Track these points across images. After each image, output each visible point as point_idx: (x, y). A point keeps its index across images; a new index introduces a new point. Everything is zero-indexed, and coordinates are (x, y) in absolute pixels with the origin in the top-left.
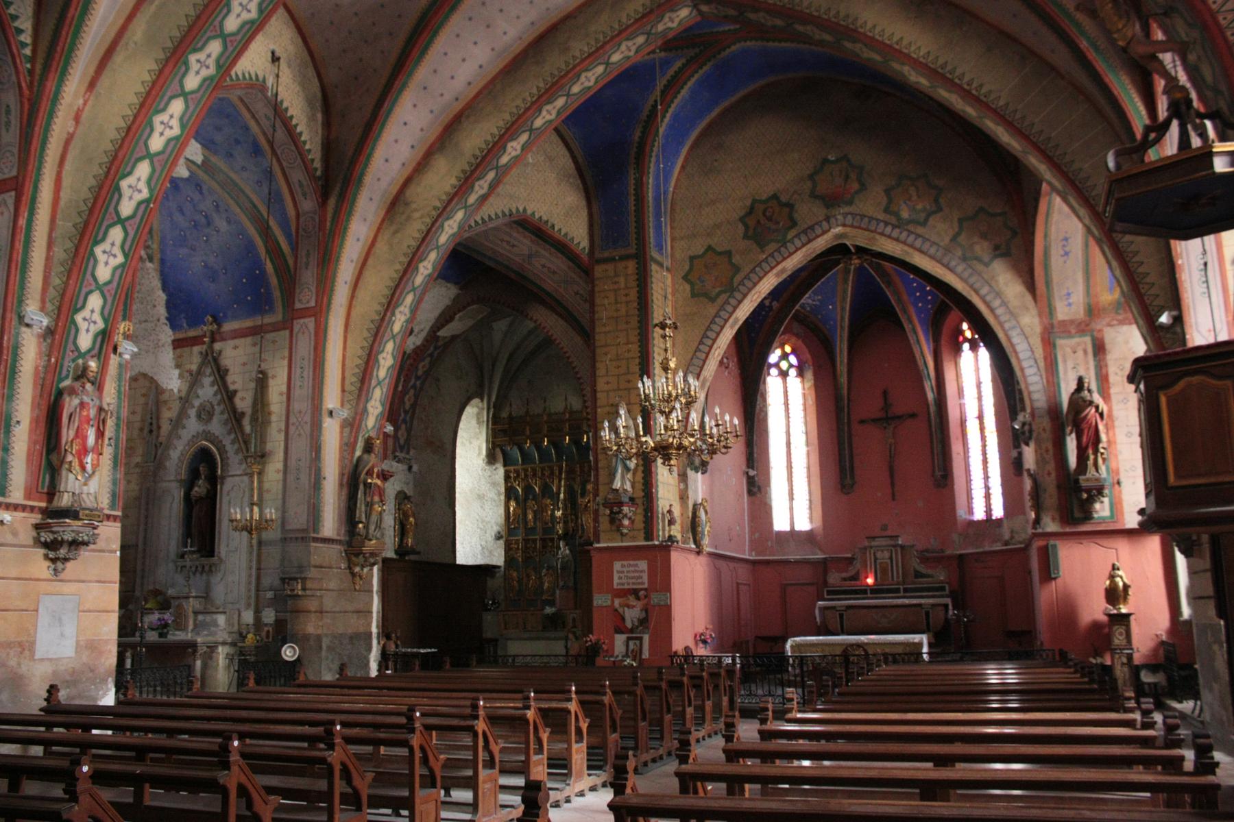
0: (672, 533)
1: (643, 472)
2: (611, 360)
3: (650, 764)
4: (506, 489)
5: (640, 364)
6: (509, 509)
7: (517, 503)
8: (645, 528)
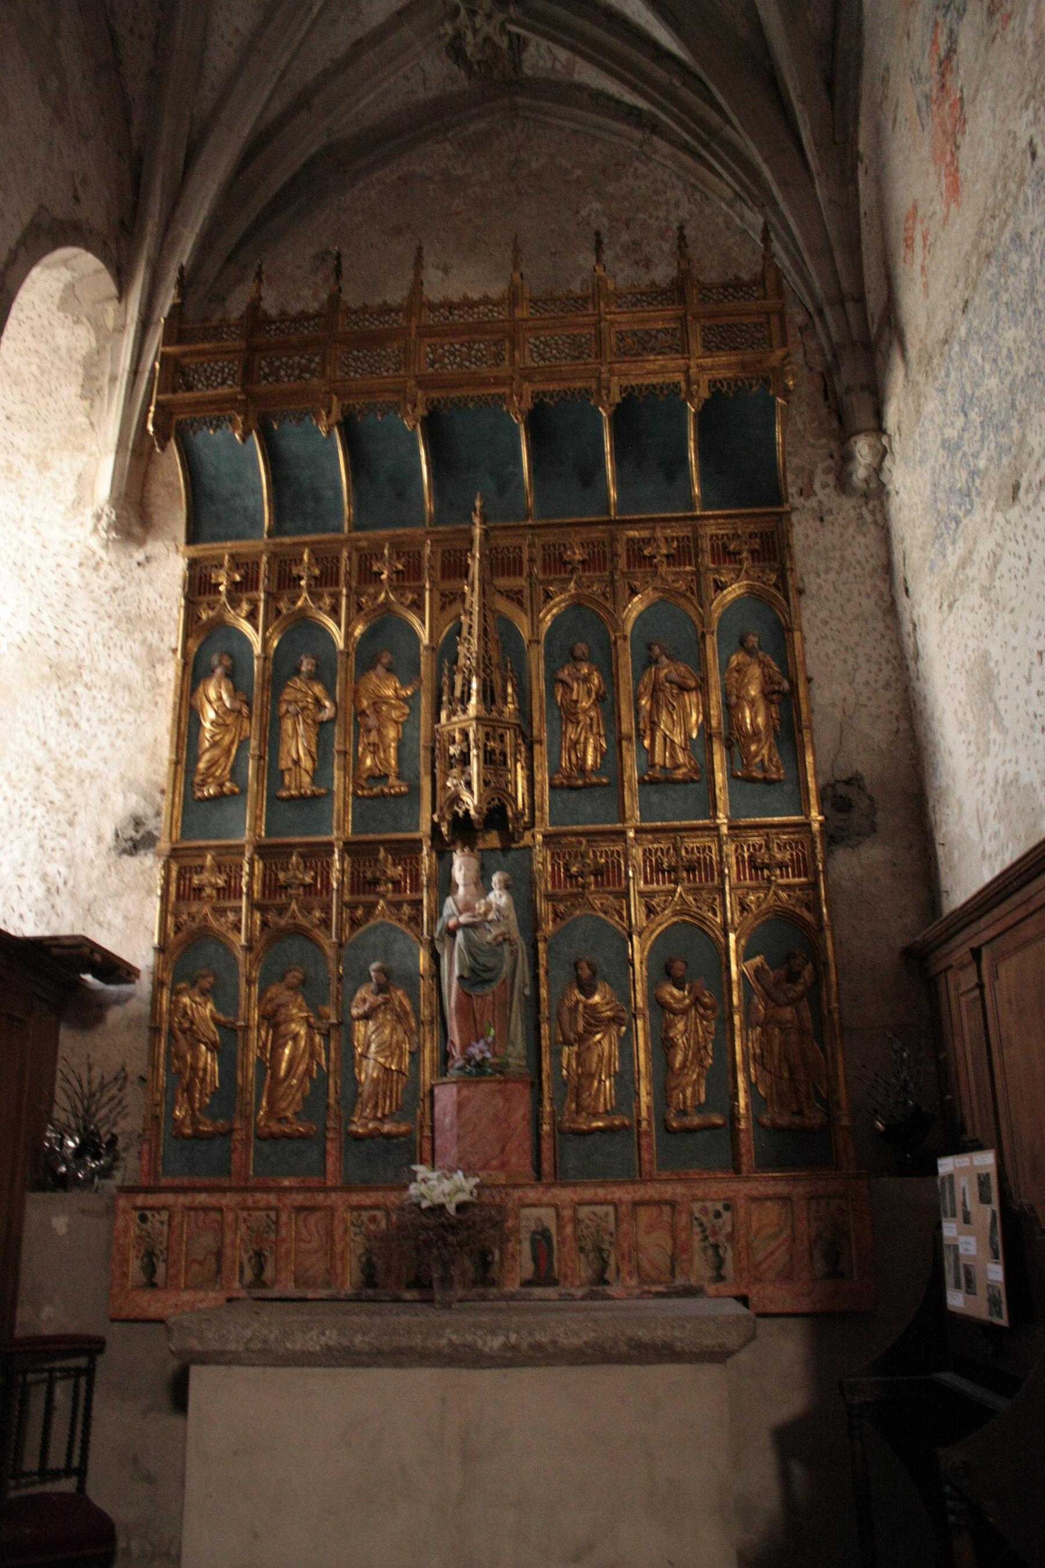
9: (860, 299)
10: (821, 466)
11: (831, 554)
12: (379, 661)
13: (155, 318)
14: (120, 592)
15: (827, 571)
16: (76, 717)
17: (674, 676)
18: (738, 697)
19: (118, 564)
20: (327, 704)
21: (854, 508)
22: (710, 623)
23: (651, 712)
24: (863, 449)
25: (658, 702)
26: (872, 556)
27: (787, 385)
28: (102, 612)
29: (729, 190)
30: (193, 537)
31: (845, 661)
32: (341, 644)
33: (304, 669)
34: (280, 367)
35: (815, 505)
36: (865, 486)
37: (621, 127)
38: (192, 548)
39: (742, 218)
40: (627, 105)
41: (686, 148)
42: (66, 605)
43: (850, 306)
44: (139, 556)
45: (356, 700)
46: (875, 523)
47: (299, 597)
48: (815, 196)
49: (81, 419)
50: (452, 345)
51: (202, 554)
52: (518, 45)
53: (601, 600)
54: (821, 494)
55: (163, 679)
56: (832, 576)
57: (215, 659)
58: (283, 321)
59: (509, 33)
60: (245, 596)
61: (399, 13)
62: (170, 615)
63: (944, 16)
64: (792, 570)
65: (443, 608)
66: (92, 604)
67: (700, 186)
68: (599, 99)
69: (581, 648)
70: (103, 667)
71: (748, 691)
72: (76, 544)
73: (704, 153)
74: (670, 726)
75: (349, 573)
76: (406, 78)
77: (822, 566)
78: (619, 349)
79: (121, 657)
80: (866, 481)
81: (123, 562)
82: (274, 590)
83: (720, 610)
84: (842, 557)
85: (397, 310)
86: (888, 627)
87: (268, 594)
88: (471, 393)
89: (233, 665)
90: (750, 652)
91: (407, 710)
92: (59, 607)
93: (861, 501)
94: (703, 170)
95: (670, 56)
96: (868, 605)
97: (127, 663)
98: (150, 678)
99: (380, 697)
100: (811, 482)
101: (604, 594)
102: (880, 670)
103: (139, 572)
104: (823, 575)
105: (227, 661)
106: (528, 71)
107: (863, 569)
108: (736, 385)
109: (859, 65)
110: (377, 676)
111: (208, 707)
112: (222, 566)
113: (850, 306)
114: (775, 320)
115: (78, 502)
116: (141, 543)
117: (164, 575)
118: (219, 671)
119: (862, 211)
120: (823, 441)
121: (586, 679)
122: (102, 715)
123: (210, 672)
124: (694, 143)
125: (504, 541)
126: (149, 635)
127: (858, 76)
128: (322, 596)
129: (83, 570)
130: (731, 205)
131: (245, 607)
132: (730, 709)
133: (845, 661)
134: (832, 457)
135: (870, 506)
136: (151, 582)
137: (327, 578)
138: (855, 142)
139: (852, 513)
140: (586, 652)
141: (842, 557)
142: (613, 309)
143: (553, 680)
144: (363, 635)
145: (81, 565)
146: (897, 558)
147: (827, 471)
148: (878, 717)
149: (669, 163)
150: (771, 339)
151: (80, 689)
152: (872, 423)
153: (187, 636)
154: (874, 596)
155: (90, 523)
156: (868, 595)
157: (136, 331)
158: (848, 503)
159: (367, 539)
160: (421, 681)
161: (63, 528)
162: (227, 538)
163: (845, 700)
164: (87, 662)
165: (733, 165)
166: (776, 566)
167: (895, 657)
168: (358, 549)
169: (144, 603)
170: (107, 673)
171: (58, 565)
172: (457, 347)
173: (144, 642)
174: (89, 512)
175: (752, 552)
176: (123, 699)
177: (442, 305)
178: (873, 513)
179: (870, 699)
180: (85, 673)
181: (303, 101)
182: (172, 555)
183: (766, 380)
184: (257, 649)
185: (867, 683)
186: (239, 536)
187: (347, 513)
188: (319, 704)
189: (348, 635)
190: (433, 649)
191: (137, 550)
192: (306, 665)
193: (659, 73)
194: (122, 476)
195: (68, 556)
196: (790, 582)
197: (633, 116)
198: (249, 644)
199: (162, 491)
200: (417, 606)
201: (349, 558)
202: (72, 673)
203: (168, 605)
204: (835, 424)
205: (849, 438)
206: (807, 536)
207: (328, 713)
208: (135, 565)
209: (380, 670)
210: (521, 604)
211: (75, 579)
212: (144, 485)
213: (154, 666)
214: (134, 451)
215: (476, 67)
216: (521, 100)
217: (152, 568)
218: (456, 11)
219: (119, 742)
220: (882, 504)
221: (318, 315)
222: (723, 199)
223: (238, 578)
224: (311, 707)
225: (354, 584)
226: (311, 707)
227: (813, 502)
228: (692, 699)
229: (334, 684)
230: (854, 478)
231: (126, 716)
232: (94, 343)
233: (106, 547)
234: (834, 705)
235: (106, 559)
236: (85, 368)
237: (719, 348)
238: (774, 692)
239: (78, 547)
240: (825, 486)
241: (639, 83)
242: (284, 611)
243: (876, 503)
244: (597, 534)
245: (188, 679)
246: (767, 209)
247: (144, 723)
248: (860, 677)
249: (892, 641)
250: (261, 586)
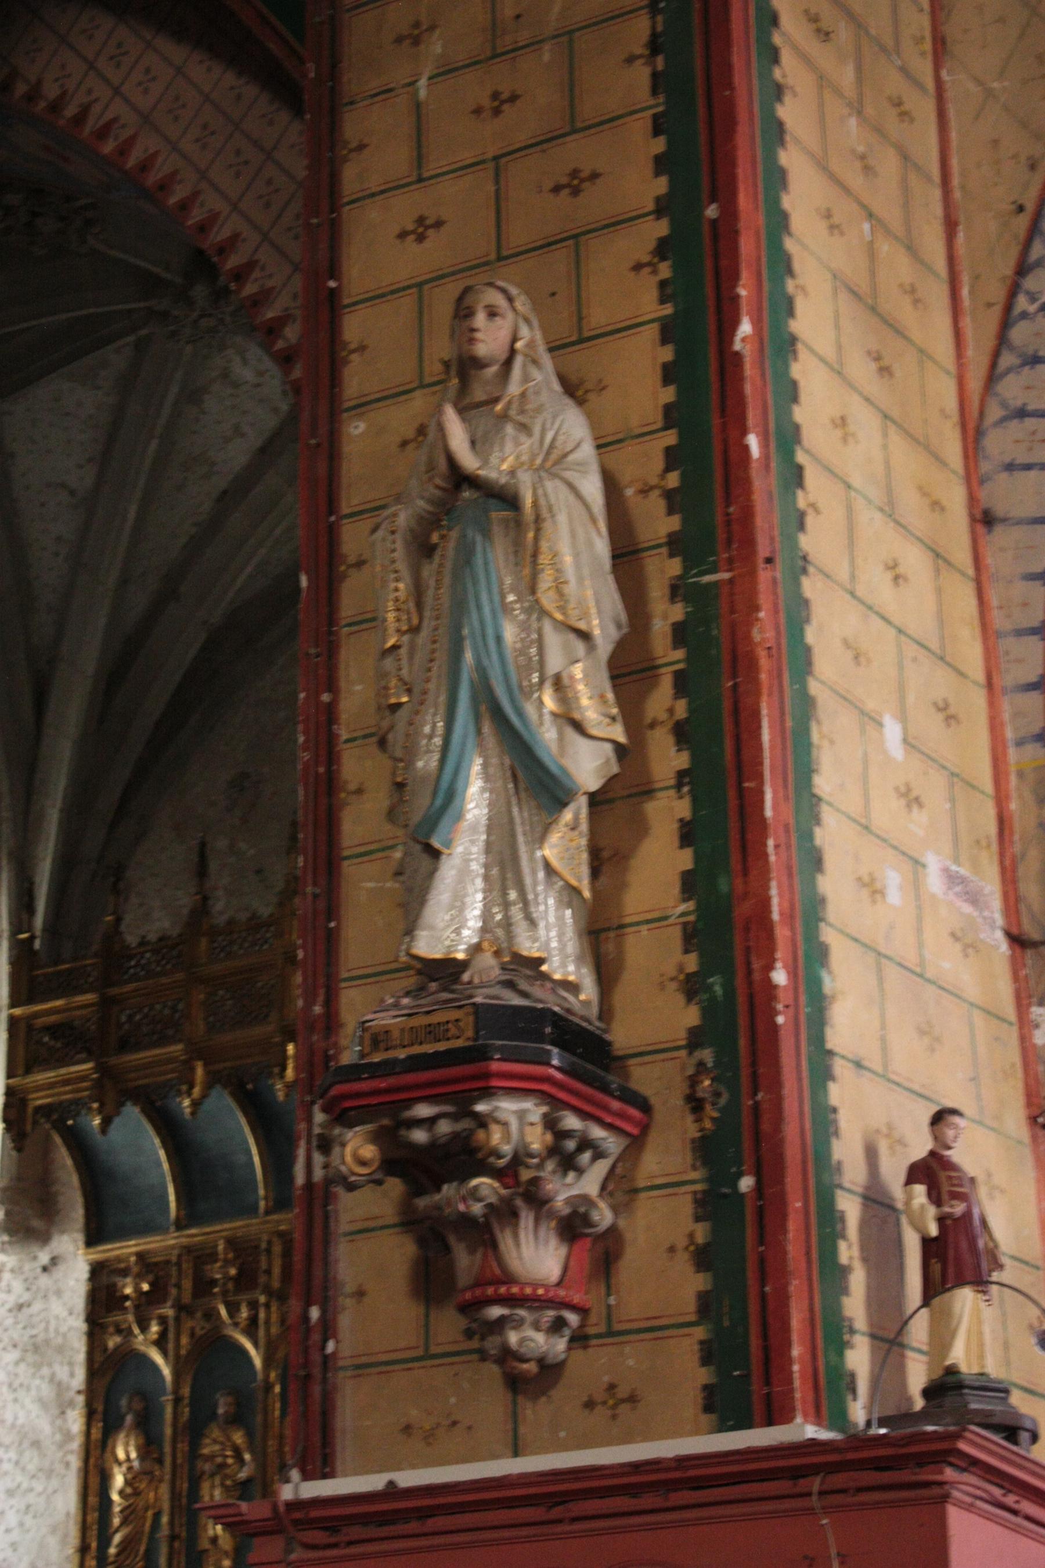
0: (959, 1355)
1: (687, 835)
2: (446, 71)
3: (814, 26)
4: (93, 1371)
5: (655, 46)
6: (105, 1479)
7: (150, 1447)
8: (706, 1305)
33: (221, 1411)
38: (91, 1250)
57: (124, 1402)
61: (262, 450)
63: (16, 1418)
81: (27, 1267)
97: (35, 1409)
98: (60, 1429)
103: (44, 1281)
118: (129, 1419)
126: (57, 1368)
136: (59, 1293)
137: (246, 1280)
170: (13, 1426)
173: (52, 1378)
176: (32, 1461)
208: (39, 1270)
217: (58, 1272)
219: (29, 1521)
223: (145, 1287)
247: (55, 1492)
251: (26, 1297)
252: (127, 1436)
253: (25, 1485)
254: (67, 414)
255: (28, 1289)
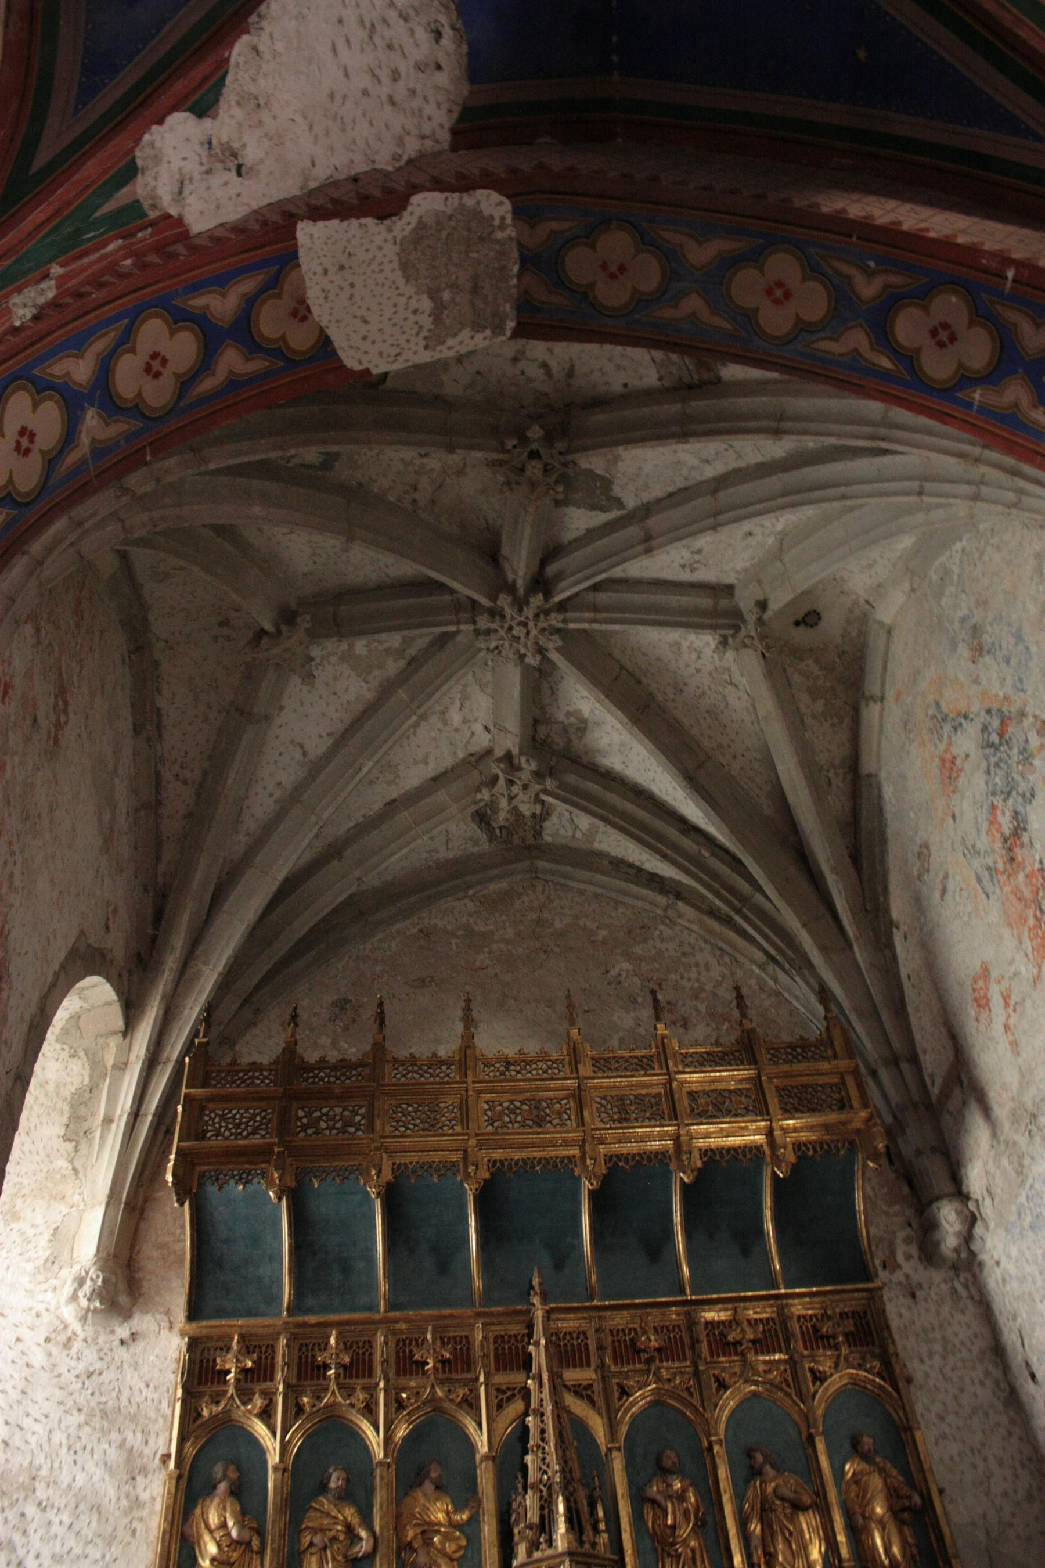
9: (914, 1059)
10: (901, 1235)
11: (931, 1336)
12: (427, 1476)
13: (164, 1057)
14: (95, 1376)
15: (931, 1354)
16: (21, 1552)
17: (786, 1492)
18: (864, 1517)
19: (95, 1340)
20: (363, 1534)
21: (945, 1281)
22: (815, 1421)
23: (763, 1539)
24: (948, 1216)
25: (770, 1526)
26: (976, 1336)
27: (876, 1148)
28: (70, 1403)
29: (761, 954)
30: (194, 1313)
31: (974, 1467)
32: (379, 1453)
33: (332, 1485)
34: (320, 1118)
35: (903, 1279)
36: (955, 1255)
37: (644, 892)
38: (194, 1325)
39: (775, 980)
40: (648, 872)
41: (712, 913)
42: (24, 1392)
43: (905, 1066)
44: (123, 1331)
45: (399, 1529)
46: (971, 1298)
47: (326, 1389)
48: (855, 960)
49: (62, 1164)
50: (512, 1102)
51: (205, 1332)
52: (547, 812)
53: (685, 1395)
54: (907, 1267)
55: (145, 1496)
56: (937, 1361)
57: (218, 1470)
58: (321, 1069)
59: (543, 802)
60: (258, 1387)
61: (434, 779)
62: (158, 1410)
63: (1004, 800)
64: (897, 1355)
65: (500, 1407)
66: (58, 1392)
67: (727, 948)
68: (620, 866)
69: (670, 1458)
70: (65, 1479)
71: (873, 1510)
72: (44, 1314)
73: (737, 918)
74: (789, 1558)
75: (385, 1361)
76: (432, 839)
77: (924, 1350)
78: (693, 1110)
79: (90, 1466)
80: (956, 1250)
82: (294, 1381)
83: (823, 1406)
84: (943, 1338)
85: (448, 1063)
86: (1012, 1422)
87: (287, 1385)
88: (538, 1155)
89: (239, 1478)
90: (866, 1457)
91: (464, 1543)
92: (14, 1395)
93: (951, 1273)
94: (731, 935)
95: (697, 830)
96: (985, 1394)
97: (99, 1473)
98: (128, 1496)
99: (430, 1523)
100: (893, 1253)
101: (688, 1389)
102: (1017, 1476)
103: (121, 1353)
104: (926, 1360)
105: (233, 1474)
106: (548, 839)
107: (970, 1351)
108: (822, 1148)
109: (884, 841)
110: (425, 1495)
111: (207, 1538)
112: (229, 1349)
113: (905, 1066)
114: (850, 1081)
115: (52, 1261)
116: (126, 1315)
117: (152, 1358)
118: (222, 1487)
119: (904, 974)
120: (897, 1208)
121: (681, 1497)
122: (58, 1549)
123: (209, 1489)
124: (725, 908)
125: (568, 1324)
126: (130, 1436)
127: (884, 852)
128: (354, 1390)
129: (50, 1346)
130: (762, 967)
131: (258, 1402)
132: (857, 1533)
133: (974, 1467)
134: (910, 1225)
135: (962, 1279)
136: (135, 1366)
138: (887, 910)
139: (944, 1286)
140: (676, 1460)
141: (943, 1338)
142: (680, 1068)
143: (640, 1499)
144: (405, 1439)
145: (47, 1340)
146: (1010, 1337)
147: (908, 1241)
148: (1029, 1539)
149: (695, 927)
150: (850, 1101)
151: (31, 1510)
152: (950, 1188)
153: (182, 1439)
154: (989, 1383)
155: (68, 1289)
156: (982, 1383)
157: (142, 1070)
158: (938, 1276)
159: (407, 1320)
160: (479, 1503)
161: (30, 1292)
162: (235, 1314)
163: (985, 1516)
164: (44, 1472)
165: (767, 930)
166: (877, 1351)
167: (1030, 1460)
168: (394, 1332)
169: (126, 1393)
170: (69, 1487)
171: (18, 1340)
172: (518, 1104)
174: (67, 1276)
175: (846, 1335)
176: (89, 1526)
177: (498, 1060)
178: (966, 1286)
179: (1013, 1515)
180: (40, 1486)
181: (334, 851)
182: (165, 1333)
183: (852, 1143)
184: (273, 1458)
185: (1005, 1494)
186: (250, 1313)
187: (383, 1289)
188: (352, 1537)
189: (388, 1439)
190: (494, 1459)
191: (121, 1325)
192: (335, 1481)
193: (688, 843)
194: (112, 1233)
195: (32, 1328)
196: (897, 1371)
197: (655, 881)
198: (261, 1451)
199: (155, 1254)
200: (470, 1404)
201: (386, 1343)
202: (22, 1486)
203: (156, 1396)
204: (906, 1190)
205: (930, 1203)
206: (901, 1316)
207: (364, 1546)
208: (117, 1342)
209: (428, 1486)
210: (592, 1402)
211: (38, 1358)
212: (132, 1246)
213: (133, 1479)
214: (127, 1204)
215: (497, 831)
216: (541, 864)
217: (138, 1347)
218: (495, 779)
220: (974, 1276)
221: (362, 1064)
222: (753, 961)
223: (250, 1364)
224: (342, 1537)
225: (391, 1375)
226: (342, 1537)
227: (898, 1276)
228: (808, 1523)
229: (370, 1506)
230: (943, 1247)
231: (90, 1549)
232: (87, 1080)
233: (83, 1319)
234: (973, 1524)
235: (82, 1335)
236: (72, 1106)
237: (797, 1110)
238: (904, 1509)
239: (46, 1318)
240: (908, 1257)
241: (669, 852)
242: (308, 1409)
243: (968, 1275)
244: (674, 1315)
245: (181, 1497)
246: (806, 972)
248: (997, 1486)
249: (1021, 1439)
250: (279, 1376)
251: (98, 1365)
252: (223, 1502)
253: (77, 1551)
254: (335, 693)
255: (101, 1359)
